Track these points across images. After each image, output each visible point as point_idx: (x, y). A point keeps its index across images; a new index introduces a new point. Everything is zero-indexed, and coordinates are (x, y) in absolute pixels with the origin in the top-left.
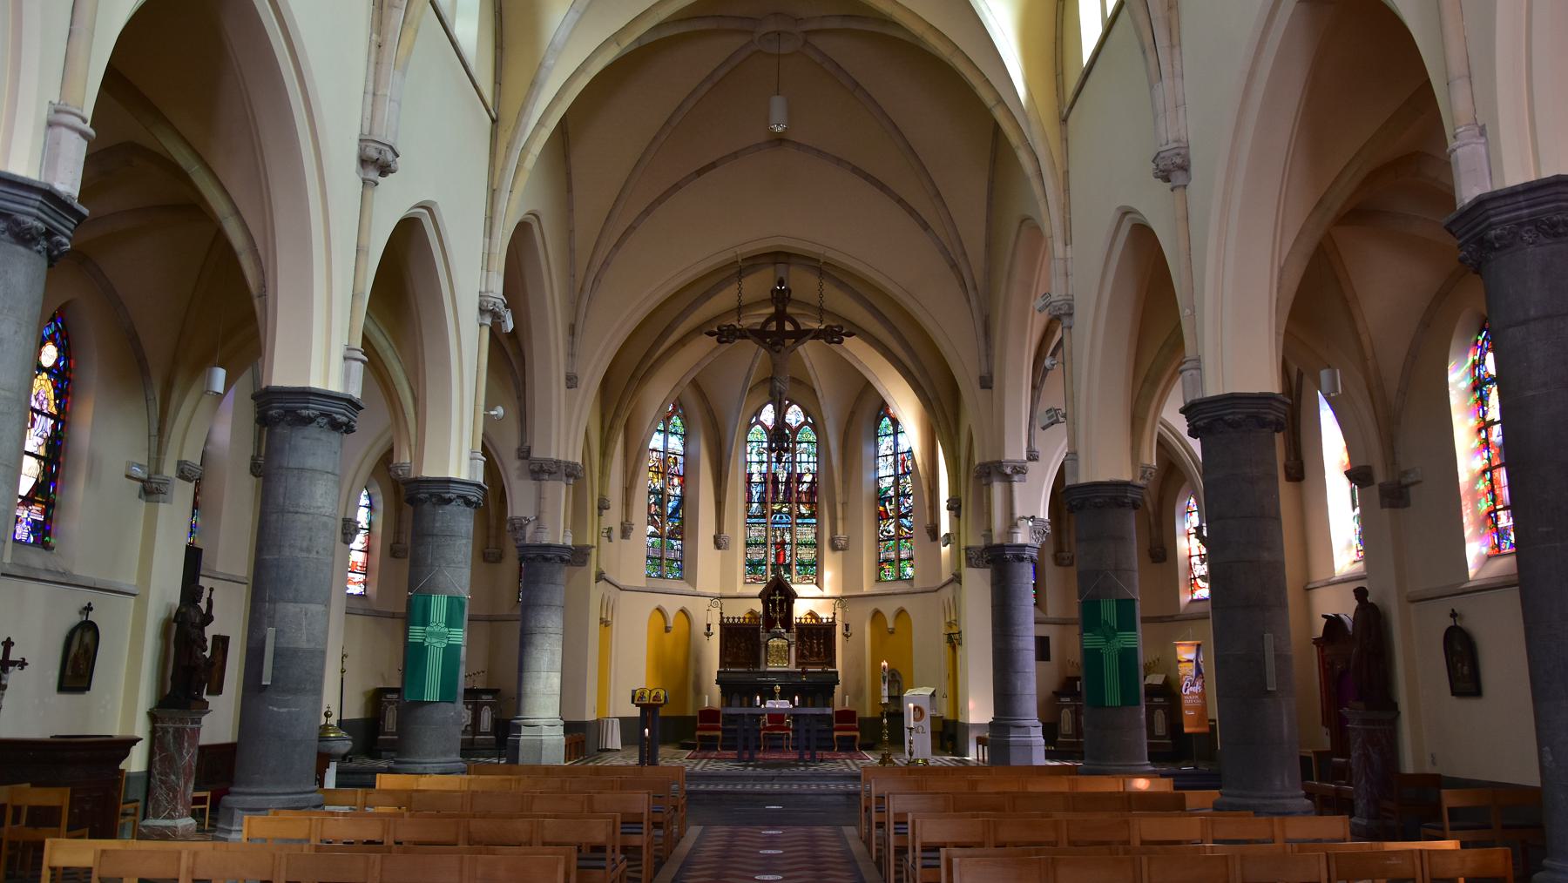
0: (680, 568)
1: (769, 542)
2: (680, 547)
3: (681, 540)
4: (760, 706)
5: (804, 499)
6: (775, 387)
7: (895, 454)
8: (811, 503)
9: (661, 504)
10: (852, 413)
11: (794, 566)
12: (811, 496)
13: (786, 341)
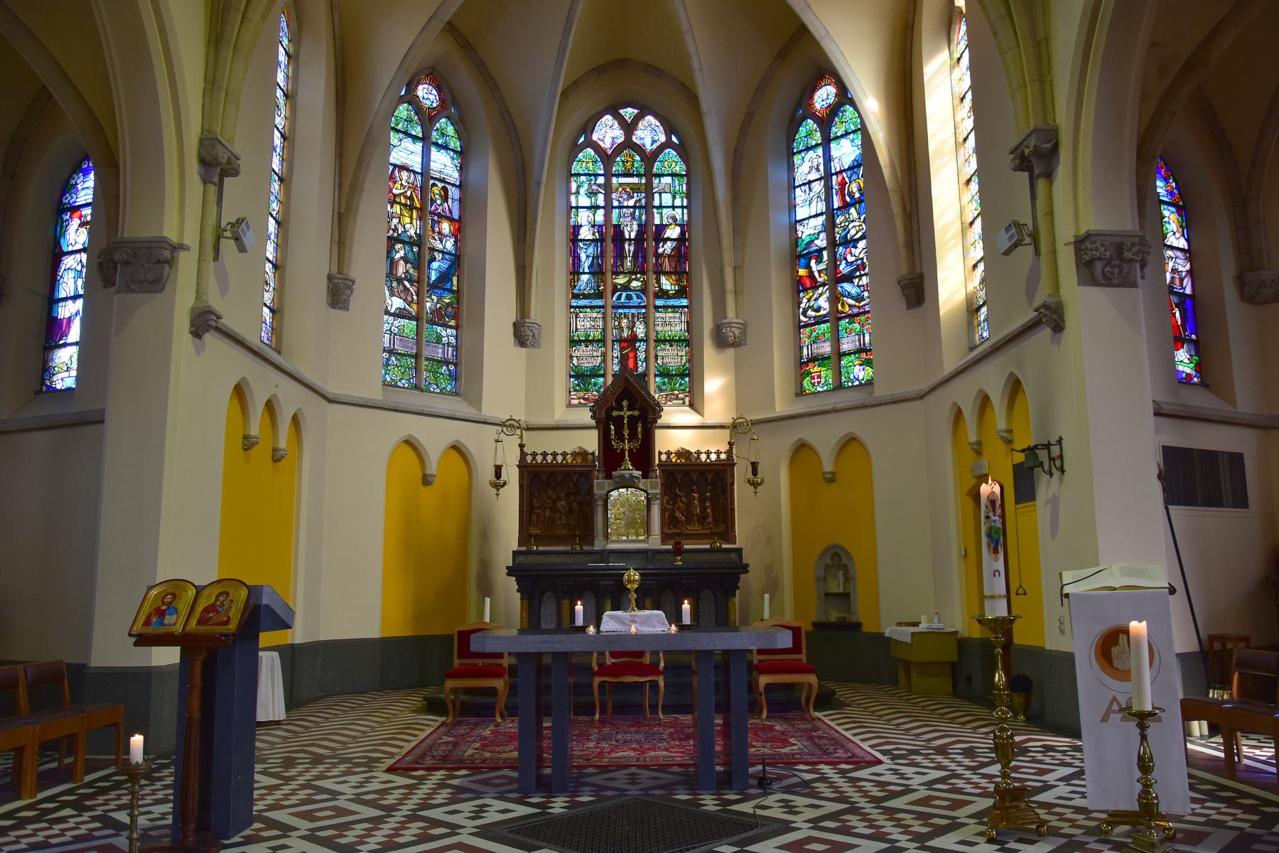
0: (454, 377)
1: (609, 338)
2: (453, 340)
3: (456, 328)
4: (582, 629)
5: (667, 266)
7: (827, 176)
8: (679, 273)
9: (419, 262)
10: (749, 116)
11: (652, 376)
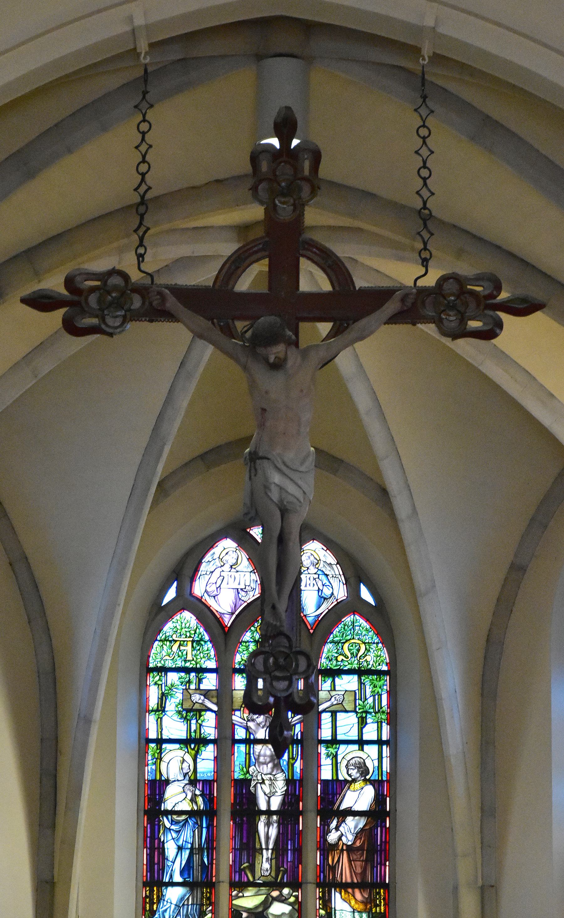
6: (266, 488)
12: (369, 860)
13: (304, 326)
